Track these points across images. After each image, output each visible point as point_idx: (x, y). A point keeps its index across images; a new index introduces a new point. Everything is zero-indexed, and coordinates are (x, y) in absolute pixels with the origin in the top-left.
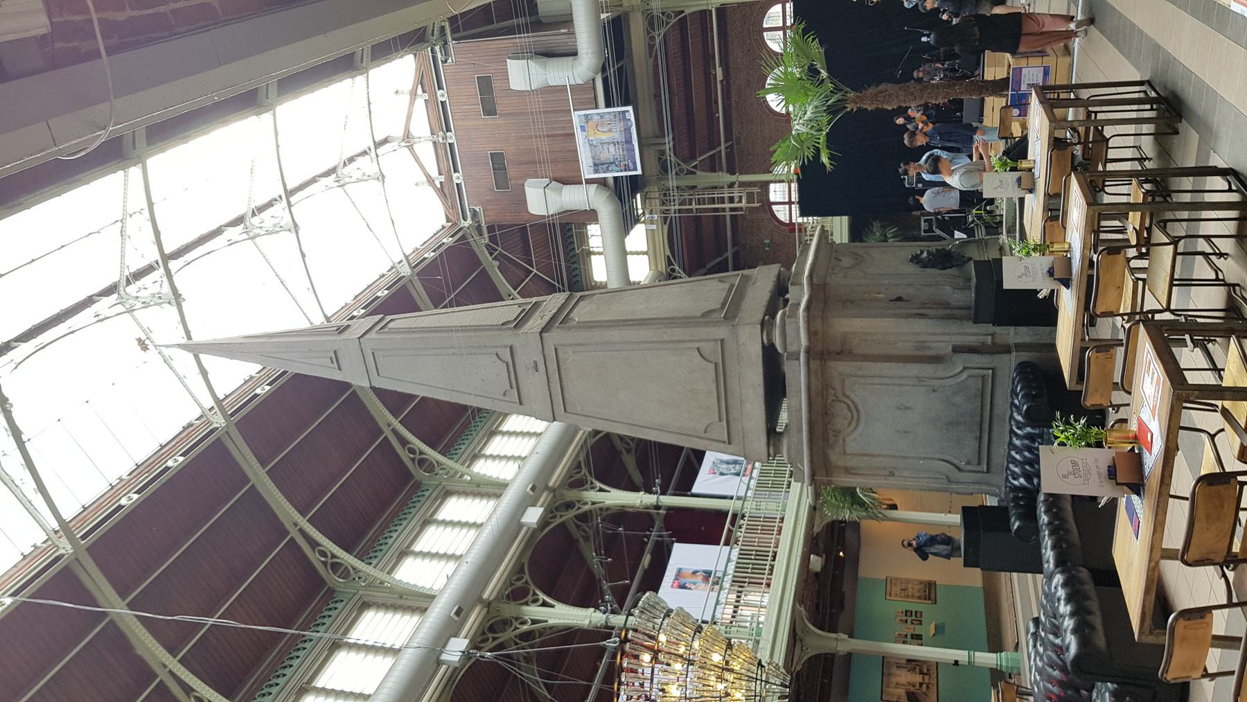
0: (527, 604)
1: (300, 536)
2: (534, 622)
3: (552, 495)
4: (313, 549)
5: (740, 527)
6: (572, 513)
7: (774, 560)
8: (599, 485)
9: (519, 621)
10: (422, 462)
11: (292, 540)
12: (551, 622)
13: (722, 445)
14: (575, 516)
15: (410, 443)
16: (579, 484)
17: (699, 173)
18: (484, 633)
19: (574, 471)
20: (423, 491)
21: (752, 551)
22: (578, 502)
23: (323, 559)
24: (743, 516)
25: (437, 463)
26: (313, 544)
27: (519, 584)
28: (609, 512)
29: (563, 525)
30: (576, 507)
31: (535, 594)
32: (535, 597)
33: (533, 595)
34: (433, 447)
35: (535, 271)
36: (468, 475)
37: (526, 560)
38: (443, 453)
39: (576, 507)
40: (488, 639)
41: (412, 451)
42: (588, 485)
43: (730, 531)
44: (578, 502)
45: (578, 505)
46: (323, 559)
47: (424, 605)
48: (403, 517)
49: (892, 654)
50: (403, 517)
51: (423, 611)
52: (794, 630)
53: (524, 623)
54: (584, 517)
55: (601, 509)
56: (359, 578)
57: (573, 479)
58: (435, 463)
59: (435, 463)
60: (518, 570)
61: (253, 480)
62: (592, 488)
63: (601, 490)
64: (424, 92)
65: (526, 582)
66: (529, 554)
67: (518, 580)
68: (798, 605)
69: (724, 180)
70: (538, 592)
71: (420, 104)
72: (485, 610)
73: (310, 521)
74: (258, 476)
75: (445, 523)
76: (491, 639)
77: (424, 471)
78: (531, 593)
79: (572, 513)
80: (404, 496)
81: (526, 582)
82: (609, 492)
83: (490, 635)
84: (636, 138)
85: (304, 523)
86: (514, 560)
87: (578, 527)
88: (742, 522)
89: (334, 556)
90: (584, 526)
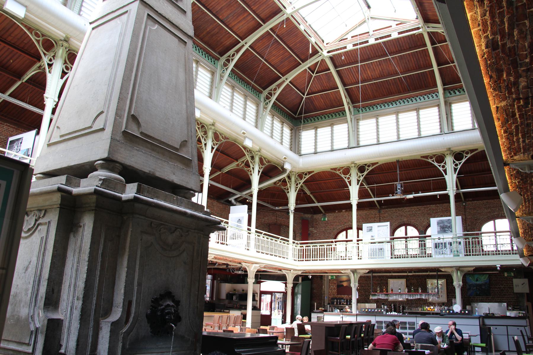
1: (241, 45)
4: (277, 86)
6: (249, 159)
7: (275, 256)
8: (261, 171)
9: (205, 138)
10: (228, 61)
11: (240, 42)
13: (48, 140)
14: (248, 161)
15: (237, 54)
17: (358, 186)
18: (201, 123)
21: (225, 234)
23: (231, 56)
24: (288, 244)
25: (228, 68)
26: (238, 51)
28: (250, 176)
29: (245, 155)
31: (217, 144)
34: (235, 66)
35: (305, 97)
36: (265, 114)
38: (232, 70)
40: (199, 126)
41: (233, 55)
46: (231, 56)
47: (293, 149)
48: (275, 107)
50: (275, 107)
51: (210, 97)
54: (247, 165)
56: (224, 70)
58: (270, 100)
59: (270, 100)
61: (264, 26)
62: (214, 144)
63: (259, 172)
64: (397, 25)
65: (265, 164)
67: (222, 137)
68: (214, 255)
69: (354, 200)
70: (217, 146)
71: (387, 24)
72: (63, 39)
73: (247, 49)
74: (266, 28)
75: (245, 104)
76: (198, 127)
77: (224, 62)
79: (249, 159)
80: (216, 56)
82: (212, 152)
83: (200, 126)
85: (246, 47)
87: (243, 162)
89: (232, 60)
90: (243, 164)
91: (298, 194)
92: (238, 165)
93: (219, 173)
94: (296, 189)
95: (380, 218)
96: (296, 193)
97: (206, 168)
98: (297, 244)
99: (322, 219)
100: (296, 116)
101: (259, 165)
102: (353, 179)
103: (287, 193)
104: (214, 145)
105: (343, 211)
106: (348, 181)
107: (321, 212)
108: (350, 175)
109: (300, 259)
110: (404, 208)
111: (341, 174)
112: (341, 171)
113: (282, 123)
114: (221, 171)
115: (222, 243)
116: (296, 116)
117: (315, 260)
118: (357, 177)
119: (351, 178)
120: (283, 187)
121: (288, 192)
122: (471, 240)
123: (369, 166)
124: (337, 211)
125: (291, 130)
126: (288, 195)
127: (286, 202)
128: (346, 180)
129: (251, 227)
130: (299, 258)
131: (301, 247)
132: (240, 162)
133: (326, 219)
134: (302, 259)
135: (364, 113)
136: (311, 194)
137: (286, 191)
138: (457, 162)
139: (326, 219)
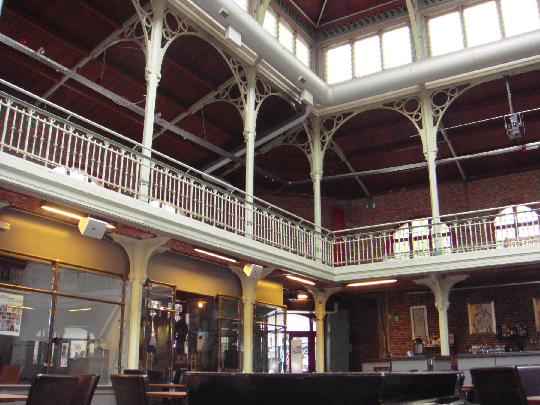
0: (164, 27)
2: (246, 96)
3: (252, 65)
5: (187, 179)
8: (260, 102)
12: (149, 43)
16: (260, 88)
18: (238, 63)
19: (269, 87)
20: (310, 31)
22: (246, 84)
27: (180, 25)
30: (242, 82)
32: (259, 98)
33: (260, 97)
37: (199, 34)
39: (242, 82)
42: (259, 94)
43: (185, 170)
44: (246, 84)
45: (244, 83)
49: (19, 258)
50: (308, 30)
52: (490, 316)
53: (148, 22)
55: (242, 103)
57: (178, 20)
60: (275, 89)
62: (257, 98)
66: (203, 38)
67: (184, 25)
76: (234, 67)
78: (262, 96)
81: (267, 93)
82: (162, 46)
83: (237, 67)
84: (468, 73)
86: (279, 86)
88: (274, 216)
90: (227, 93)
91: (327, 151)
92: (217, 97)
93: (186, 114)
94: (323, 148)
95: (467, 197)
96: (323, 153)
97: (150, 73)
98: (331, 235)
99: (367, 206)
100: (316, 24)
101: (256, 92)
102: (426, 117)
103: (307, 154)
104: (168, 36)
105: (402, 189)
106: (417, 122)
107: (364, 195)
108: (420, 111)
109: (338, 263)
110: (509, 176)
111: (403, 110)
112: (403, 105)
113: (295, 32)
114: (187, 111)
115: (173, 175)
116: (316, 24)
117: (340, 265)
118: (433, 113)
119: (421, 115)
120: (298, 145)
121: (310, 152)
122: (485, 223)
123: (453, 92)
124: (391, 191)
125: (311, 47)
126: (309, 157)
127: (307, 167)
128: (413, 120)
129: (245, 191)
130: (335, 261)
131: (339, 241)
132: (221, 89)
133: (374, 206)
134: (342, 263)
135: (438, 5)
136: (347, 160)
137: (305, 151)
138: (438, 108)
139: (374, 206)
